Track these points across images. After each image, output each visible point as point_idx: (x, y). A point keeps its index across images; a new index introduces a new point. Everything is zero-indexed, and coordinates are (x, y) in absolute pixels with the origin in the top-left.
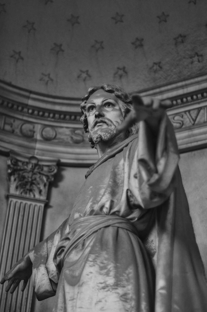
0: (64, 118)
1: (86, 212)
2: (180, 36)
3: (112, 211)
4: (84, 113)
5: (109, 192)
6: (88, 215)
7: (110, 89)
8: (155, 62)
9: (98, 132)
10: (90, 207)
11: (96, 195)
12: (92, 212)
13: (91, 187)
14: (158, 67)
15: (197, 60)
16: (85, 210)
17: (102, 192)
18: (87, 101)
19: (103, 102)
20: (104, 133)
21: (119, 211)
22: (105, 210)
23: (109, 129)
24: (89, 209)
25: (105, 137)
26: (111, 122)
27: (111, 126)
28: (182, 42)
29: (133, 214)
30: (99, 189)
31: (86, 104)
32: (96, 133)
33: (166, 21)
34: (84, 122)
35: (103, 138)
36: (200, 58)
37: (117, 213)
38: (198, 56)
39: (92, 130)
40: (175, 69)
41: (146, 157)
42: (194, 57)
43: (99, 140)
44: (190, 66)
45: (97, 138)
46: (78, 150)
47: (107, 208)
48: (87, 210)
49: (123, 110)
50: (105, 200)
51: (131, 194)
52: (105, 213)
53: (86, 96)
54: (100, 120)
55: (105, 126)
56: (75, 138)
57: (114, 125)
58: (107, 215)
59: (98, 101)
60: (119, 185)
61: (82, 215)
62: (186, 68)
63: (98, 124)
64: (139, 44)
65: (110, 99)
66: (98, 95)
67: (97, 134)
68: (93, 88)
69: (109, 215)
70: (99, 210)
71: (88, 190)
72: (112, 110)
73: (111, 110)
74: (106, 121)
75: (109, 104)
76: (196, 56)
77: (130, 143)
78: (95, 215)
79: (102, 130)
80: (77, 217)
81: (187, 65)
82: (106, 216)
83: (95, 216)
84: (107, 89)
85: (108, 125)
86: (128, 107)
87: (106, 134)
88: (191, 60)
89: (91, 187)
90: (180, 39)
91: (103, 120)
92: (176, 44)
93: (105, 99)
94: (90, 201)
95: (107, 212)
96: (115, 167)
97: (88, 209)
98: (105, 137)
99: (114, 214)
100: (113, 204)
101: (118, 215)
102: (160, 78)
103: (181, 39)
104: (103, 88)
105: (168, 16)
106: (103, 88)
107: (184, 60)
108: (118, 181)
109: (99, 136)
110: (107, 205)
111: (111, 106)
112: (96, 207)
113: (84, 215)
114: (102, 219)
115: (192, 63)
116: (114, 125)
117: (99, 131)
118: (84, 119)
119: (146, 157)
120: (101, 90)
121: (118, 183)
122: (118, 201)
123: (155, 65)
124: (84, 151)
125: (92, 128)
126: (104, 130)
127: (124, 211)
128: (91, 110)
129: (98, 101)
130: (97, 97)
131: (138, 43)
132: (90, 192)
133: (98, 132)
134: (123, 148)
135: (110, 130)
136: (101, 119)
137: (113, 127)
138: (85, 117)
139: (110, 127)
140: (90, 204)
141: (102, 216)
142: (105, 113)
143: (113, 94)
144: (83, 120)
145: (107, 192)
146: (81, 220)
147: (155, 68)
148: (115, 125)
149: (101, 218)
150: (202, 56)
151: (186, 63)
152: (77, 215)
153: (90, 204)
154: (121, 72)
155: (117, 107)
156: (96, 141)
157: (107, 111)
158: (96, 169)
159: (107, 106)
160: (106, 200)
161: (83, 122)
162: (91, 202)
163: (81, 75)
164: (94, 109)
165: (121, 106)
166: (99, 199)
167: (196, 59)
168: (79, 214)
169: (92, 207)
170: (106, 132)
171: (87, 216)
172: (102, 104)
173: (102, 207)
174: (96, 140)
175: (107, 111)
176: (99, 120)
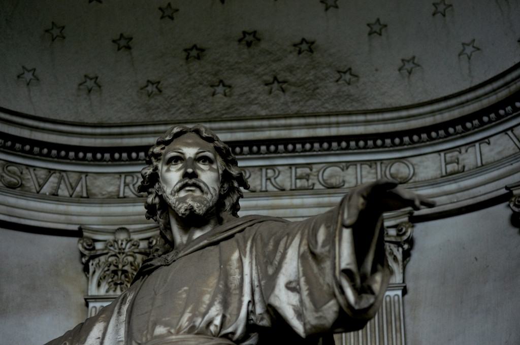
0: (49, 155)
1: (180, 327)
2: (195, 47)
3: (224, 332)
4: (155, 163)
5: (220, 300)
6: (185, 332)
7: (210, 136)
8: (150, 79)
9: (187, 201)
10: (187, 321)
11: (194, 300)
12: (192, 329)
13: (186, 288)
14: (155, 89)
15: (222, 92)
16: (180, 324)
17: (207, 298)
18: (166, 147)
19: (197, 153)
20: (199, 204)
21: (233, 333)
22: (212, 328)
23: (204, 198)
24: (187, 323)
25: (200, 210)
26: (208, 188)
27: (207, 194)
28: (198, 58)
29: (251, 340)
30: (202, 294)
31: (163, 151)
32: (183, 200)
33: (172, 18)
34: (148, 177)
35: (197, 211)
36: (228, 90)
37: (230, 336)
38: (224, 85)
39: (174, 195)
40: (185, 98)
41: (353, 267)
42: (218, 86)
43: (187, 212)
44: (210, 99)
45: (186, 210)
46: (12, 200)
47: (216, 326)
48: (183, 324)
49: (221, 172)
50: (215, 313)
51: (253, 310)
52: (213, 332)
53: (168, 138)
54: (192, 182)
55: (198, 193)
56: (8, 178)
57: (211, 193)
58: (214, 336)
59: (190, 152)
60: (231, 291)
61: (173, 331)
62: (202, 101)
63: (188, 188)
64: (124, 43)
65: (209, 151)
66: (190, 141)
67: (186, 203)
68: (181, 129)
69: (217, 336)
70: (204, 328)
71: (180, 292)
72: (209, 170)
73: (207, 169)
74: (202, 185)
75: (205, 159)
76: (221, 86)
77: (248, 228)
78: (198, 334)
79: (194, 199)
80: (162, 333)
81: (205, 97)
82: (214, 338)
83: (195, 336)
84: (205, 135)
85: (202, 191)
86: (227, 169)
87: (201, 206)
88: (212, 90)
89: (186, 288)
90: (194, 53)
91: (198, 183)
92: (187, 58)
93: (201, 150)
94: (188, 311)
95: (215, 332)
96: (224, 263)
97: (185, 322)
98: (200, 210)
99: (226, 336)
100: (225, 320)
101: (231, 339)
102: (158, 108)
103: (195, 53)
104: (197, 132)
105: (177, 10)
106: (197, 132)
107: (201, 87)
108: (230, 286)
109: (189, 208)
110: (217, 321)
111: (207, 163)
112: (199, 322)
113: (178, 332)
114: (209, 342)
115: (214, 94)
116: (211, 193)
117: (189, 199)
118: (152, 173)
119: (353, 267)
120: (194, 134)
121: (230, 288)
122: (231, 316)
123: (150, 85)
124: (22, 202)
125: (175, 192)
126: (198, 199)
127: (241, 334)
128: (173, 163)
129: (190, 152)
130: (189, 145)
131: (123, 43)
132: (184, 296)
133: (187, 201)
134: (235, 233)
135: (206, 200)
136: (193, 180)
137: (209, 196)
138: (153, 170)
139: (205, 196)
140: (187, 316)
141: (208, 337)
142: (199, 172)
143: (212, 145)
144: (147, 174)
145: (218, 301)
146: (172, 339)
147: (150, 88)
148: (212, 194)
149: (206, 340)
150: (230, 87)
151: (203, 93)
152: (160, 330)
153: (187, 316)
154: (90, 83)
155: (214, 166)
156: (183, 214)
157: (202, 170)
158: (183, 259)
159: (201, 162)
160: (216, 313)
161: (147, 176)
162: (190, 312)
163: (23, 74)
164: (179, 162)
165: (219, 164)
166: (203, 309)
167: (220, 89)
168: (168, 328)
169: (191, 320)
170: (200, 202)
171: (182, 334)
172: (196, 156)
173: (210, 323)
174: (184, 213)
175: (202, 170)
176: (190, 182)
